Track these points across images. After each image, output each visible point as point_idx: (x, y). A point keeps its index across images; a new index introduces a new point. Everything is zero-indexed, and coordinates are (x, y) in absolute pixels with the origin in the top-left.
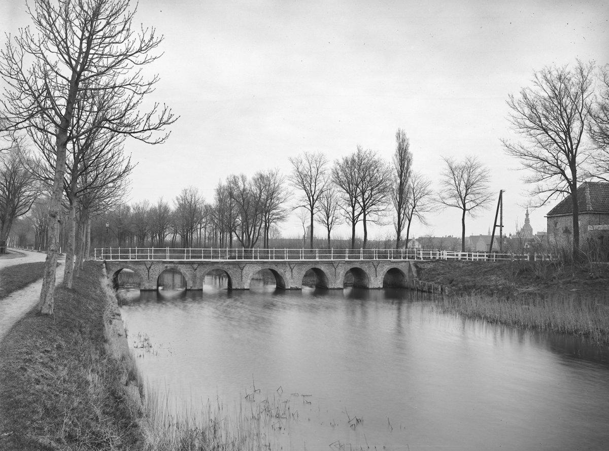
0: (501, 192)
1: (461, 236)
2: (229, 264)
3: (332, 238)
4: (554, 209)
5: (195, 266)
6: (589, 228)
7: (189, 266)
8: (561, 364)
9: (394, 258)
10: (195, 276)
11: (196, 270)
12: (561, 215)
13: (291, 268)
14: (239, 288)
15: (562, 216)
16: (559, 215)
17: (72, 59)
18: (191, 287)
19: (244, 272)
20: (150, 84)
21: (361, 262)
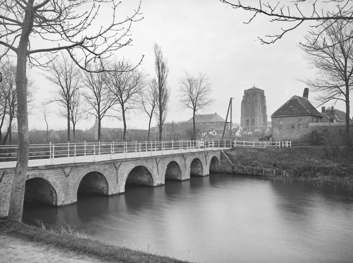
0: (231, 98)
1: (123, 128)
2: (106, 164)
3: (48, 130)
4: (276, 112)
5: (67, 170)
6: (311, 124)
7: (59, 171)
8: (327, 204)
9: (272, 145)
10: (68, 185)
11: (68, 175)
12: (285, 116)
13: (116, 167)
14: (115, 193)
15: (286, 117)
16: (282, 116)
17: (345, 94)
18: (63, 202)
19: (119, 171)
20: (94, 5)
21: (199, 153)
